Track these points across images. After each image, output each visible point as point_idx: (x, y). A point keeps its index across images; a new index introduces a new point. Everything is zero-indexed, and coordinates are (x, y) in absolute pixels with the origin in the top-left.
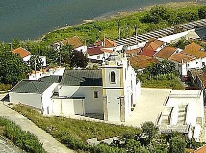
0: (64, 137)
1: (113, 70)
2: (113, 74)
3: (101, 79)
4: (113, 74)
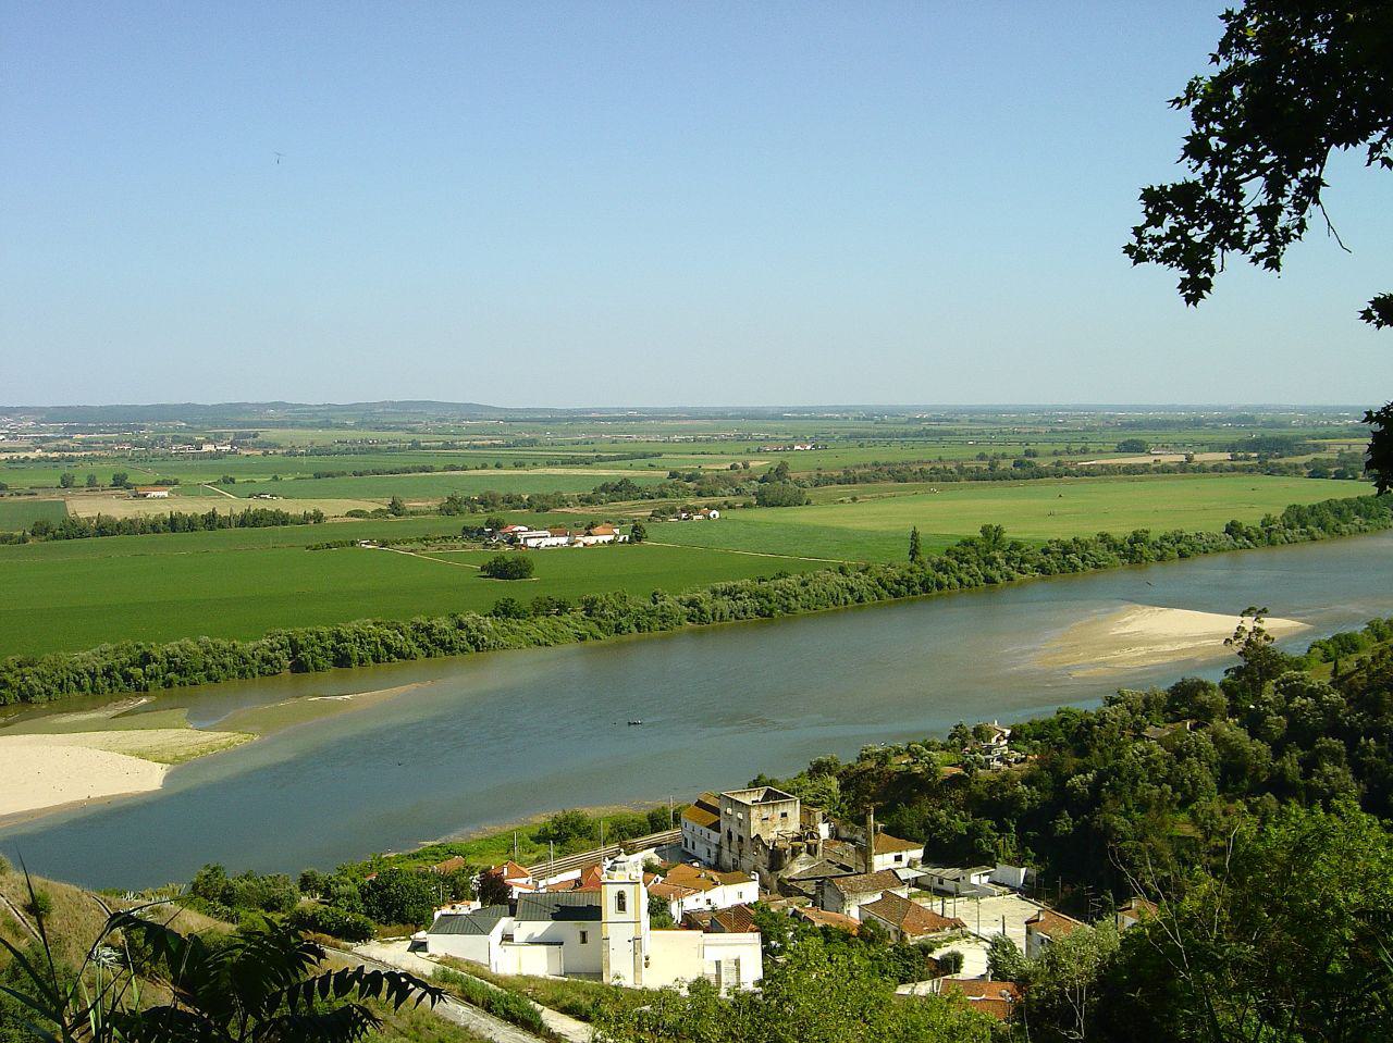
0: (566, 1003)
1: (621, 887)
2: (621, 897)
3: (601, 908)
4: (621, 897)
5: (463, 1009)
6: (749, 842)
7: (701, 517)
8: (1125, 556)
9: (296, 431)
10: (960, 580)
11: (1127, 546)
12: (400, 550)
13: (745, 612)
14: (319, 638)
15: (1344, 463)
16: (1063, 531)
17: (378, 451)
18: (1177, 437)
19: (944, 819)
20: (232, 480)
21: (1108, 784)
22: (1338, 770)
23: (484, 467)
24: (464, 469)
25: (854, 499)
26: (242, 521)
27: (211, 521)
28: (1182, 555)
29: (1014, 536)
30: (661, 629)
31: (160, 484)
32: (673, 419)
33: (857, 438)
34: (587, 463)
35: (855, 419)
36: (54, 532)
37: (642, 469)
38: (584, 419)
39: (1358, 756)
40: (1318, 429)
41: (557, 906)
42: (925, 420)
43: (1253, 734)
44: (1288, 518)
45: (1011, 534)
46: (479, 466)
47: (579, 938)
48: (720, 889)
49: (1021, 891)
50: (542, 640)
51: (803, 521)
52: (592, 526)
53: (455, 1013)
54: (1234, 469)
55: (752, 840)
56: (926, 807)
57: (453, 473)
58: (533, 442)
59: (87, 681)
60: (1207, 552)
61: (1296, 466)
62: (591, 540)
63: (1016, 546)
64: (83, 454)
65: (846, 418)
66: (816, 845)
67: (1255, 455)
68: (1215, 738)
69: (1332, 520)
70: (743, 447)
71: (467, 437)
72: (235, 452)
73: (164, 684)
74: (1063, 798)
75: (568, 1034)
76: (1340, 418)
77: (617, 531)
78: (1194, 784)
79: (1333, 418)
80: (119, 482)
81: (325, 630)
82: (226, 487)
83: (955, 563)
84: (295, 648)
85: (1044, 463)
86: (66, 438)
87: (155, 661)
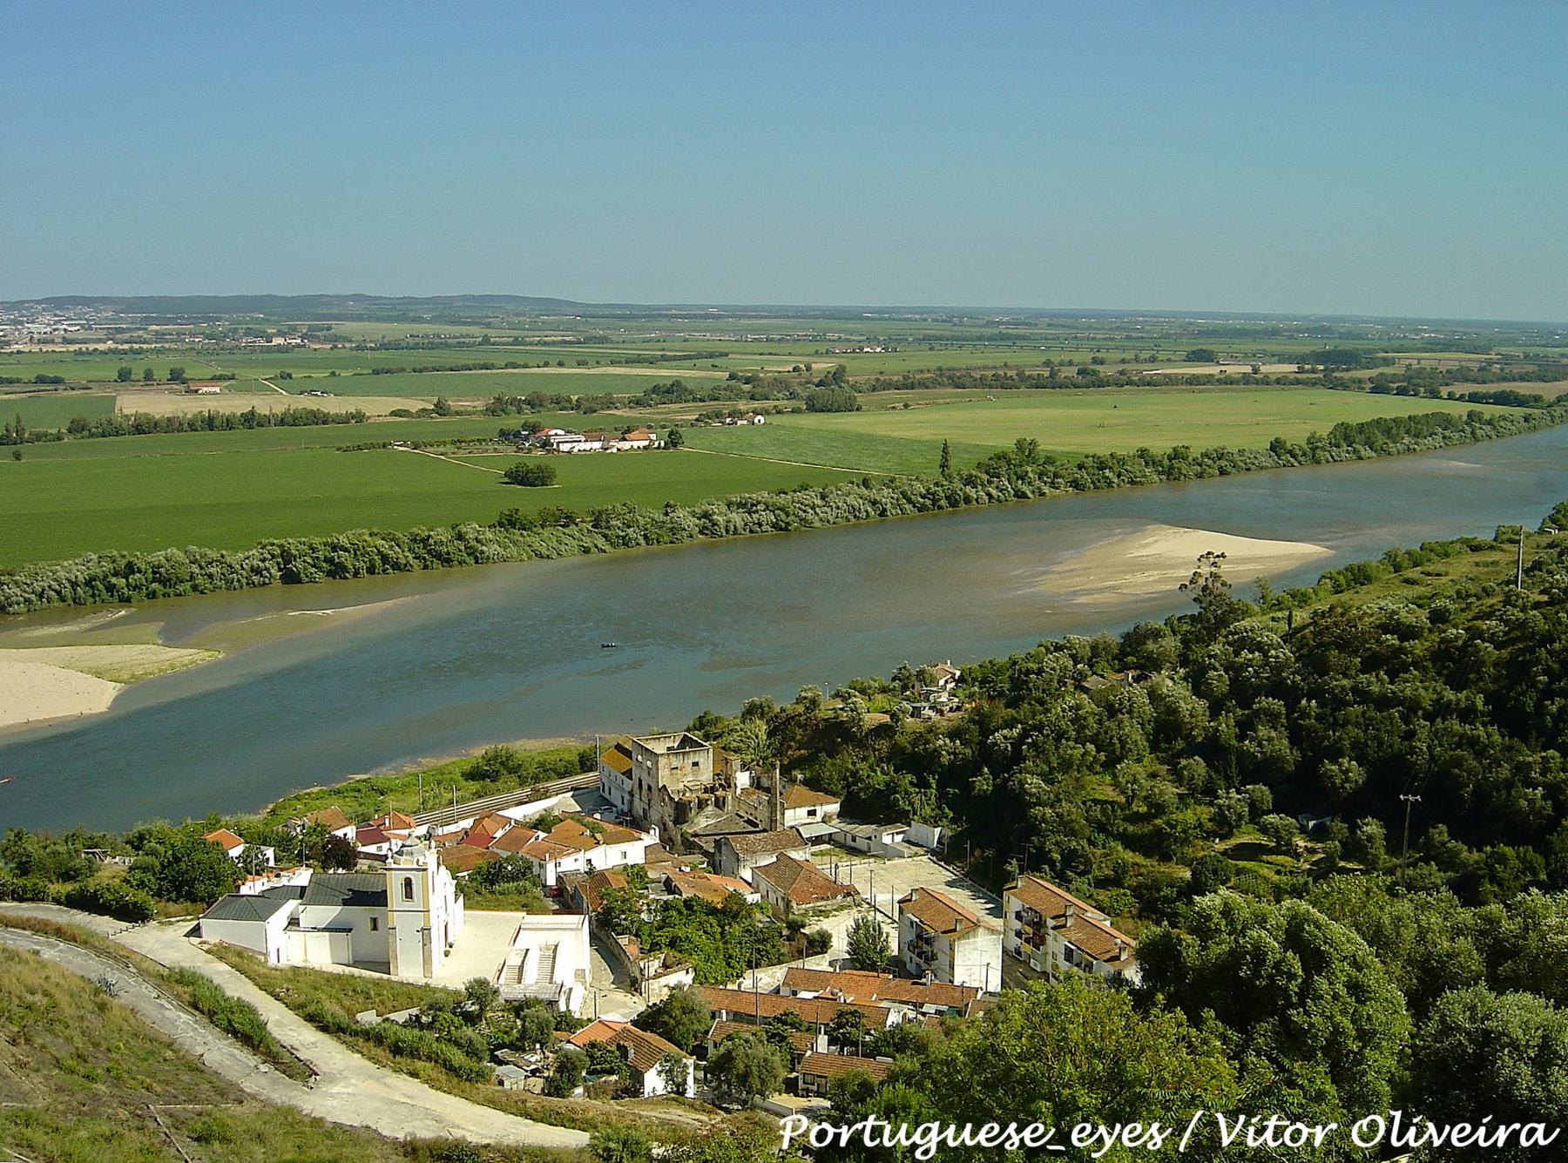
2: (408, 882)
4: (408, 882)
5: (185, 1017)
6: (657, 792)
7: (745, 422)
8: (1162, 473)
9: (373, 324)
10: (989, 494)
11: (1166, 462)
12: (431, 452)
13: (760, 525)
14: (313, 549)
15: (1408, 379)
16: (1102, 446)
17: (447, 345)
18: (1250, 347)
19: (863, 774)
20: (290, 376)
21: (1030, 740)
22: (1273, 734)
23: (546, 365)
24: (526, 366)
25: (906, 406)
26: (282, 419)
27: (250, 420)
28: (1223, 472)
29: (1050, 448)
30: (671, 542)
31: (216, 379)
32: (751, 317)
33: (931, 341)
34: (651, 362)
35: (934, 320)
36: (90, 430)
37: (706, 369)
38: (660, 315)
39: (1297, 718)
40: (1393, 342)
41: (349, 890)
42: (1003, 323)
43: (1196, 691)
44: (1335, 437)
45: (1046, 445)
46: (542, 364)
47: (369, 925)
48: (601, 849)
49: (933, 852)
50: (545, 552)
51: (849, 428)
52: (629, 431)
53: (173, 1022)
54: (1298, 382)
55: (660, 790)
56: (849, 758)
57: (514, 370)
58: (603, 340)
59: (67, 592)
60: (1248, 470)
61: (1360, 381)
62: (626, 445)
63: (1049, 460)
64: (153, 346)
65: (925, 320)
66: (724, 798)
67: (1321, 367)
68: (1154, 696)
69: (1380, 439)
70: (812, 348)
71: (537, 333)
72: (304, 346)
73: (147, 595)
74: (986, 756)
75: (300, 1047)
76: (1417, 332)
77: (653, 437)
78: (1123, 743)
79: (1410, 332)
80: (176, 376)
81: (316, 541)
82: (280, 382)
83: (985, 477)
84: (287, 557)
85: (1106, 371)
86: (139, 329)
87: (140, 572)
